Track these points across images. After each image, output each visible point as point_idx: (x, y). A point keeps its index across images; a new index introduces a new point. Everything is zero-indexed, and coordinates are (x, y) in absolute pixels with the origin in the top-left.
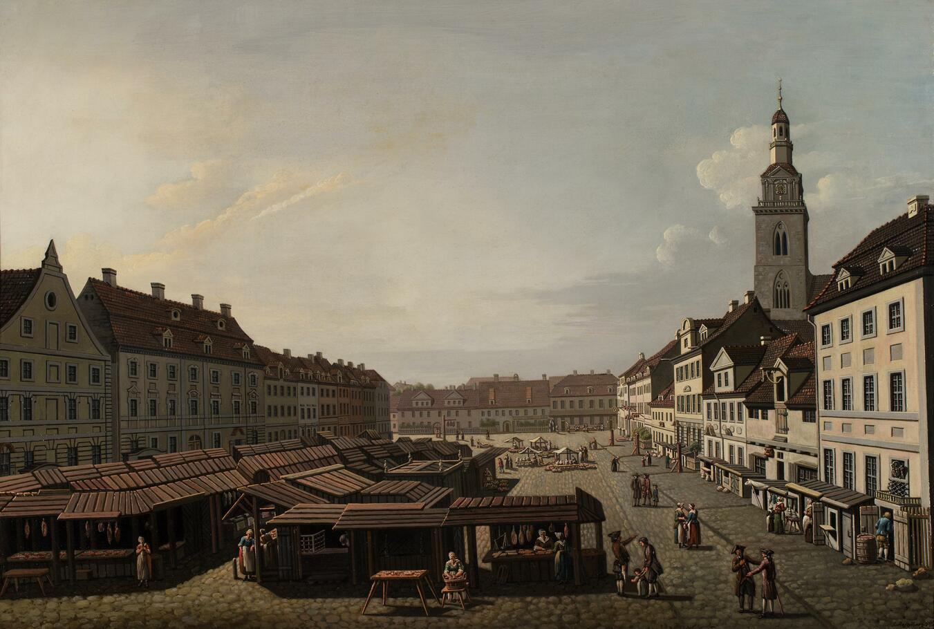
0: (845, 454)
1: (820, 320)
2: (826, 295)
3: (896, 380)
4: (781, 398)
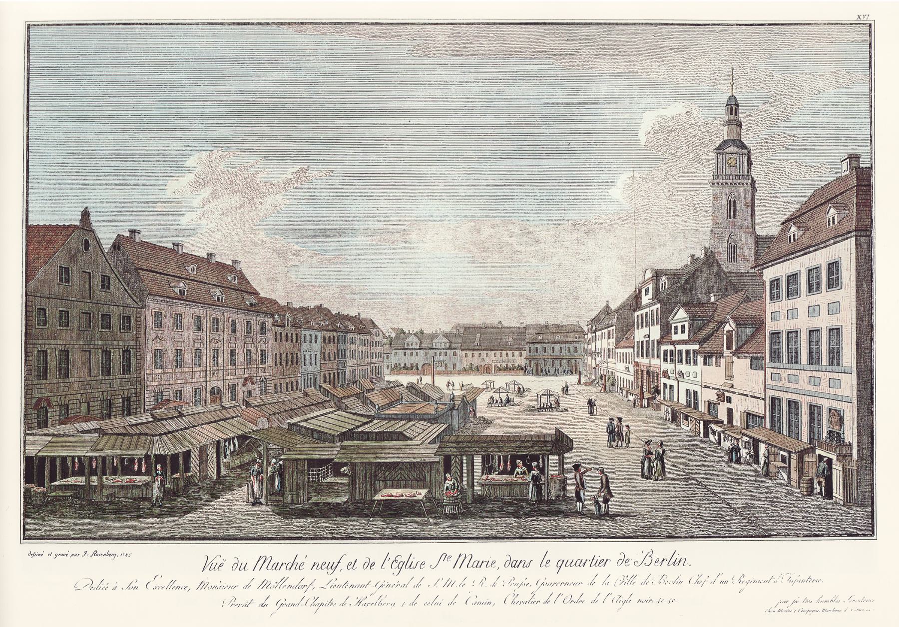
0: (811, 407)
1: (769, 274)
2: (767, 250)
3: (835, 332)
4: (729, 348)
